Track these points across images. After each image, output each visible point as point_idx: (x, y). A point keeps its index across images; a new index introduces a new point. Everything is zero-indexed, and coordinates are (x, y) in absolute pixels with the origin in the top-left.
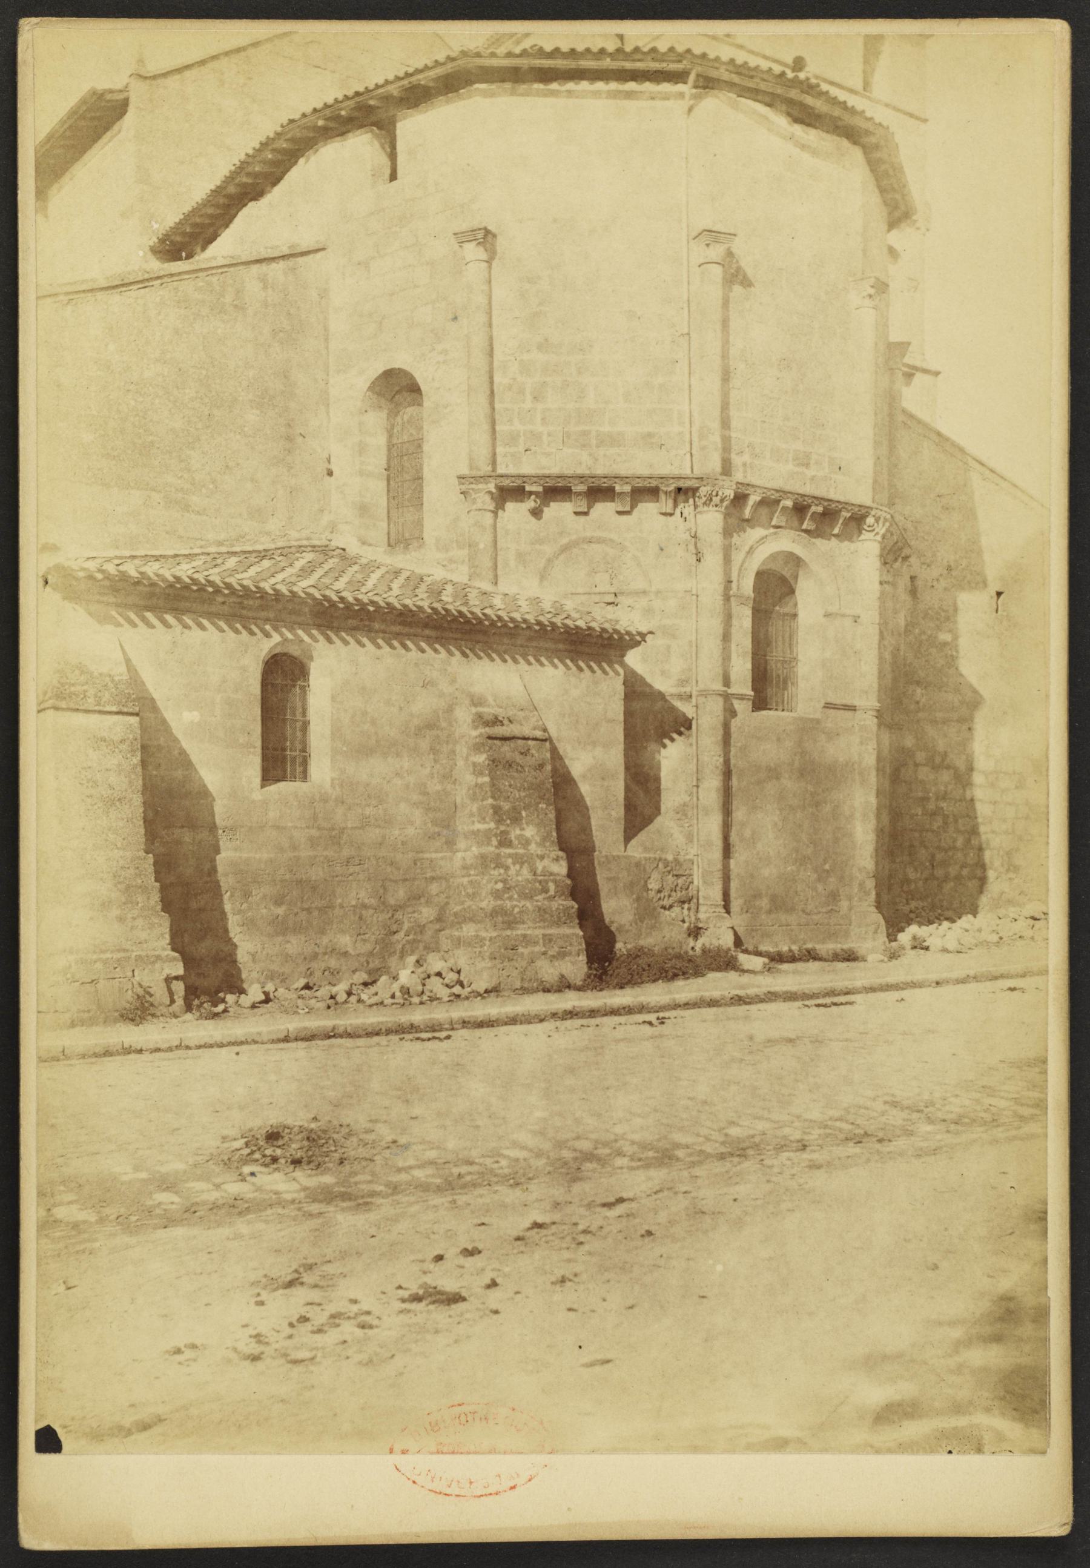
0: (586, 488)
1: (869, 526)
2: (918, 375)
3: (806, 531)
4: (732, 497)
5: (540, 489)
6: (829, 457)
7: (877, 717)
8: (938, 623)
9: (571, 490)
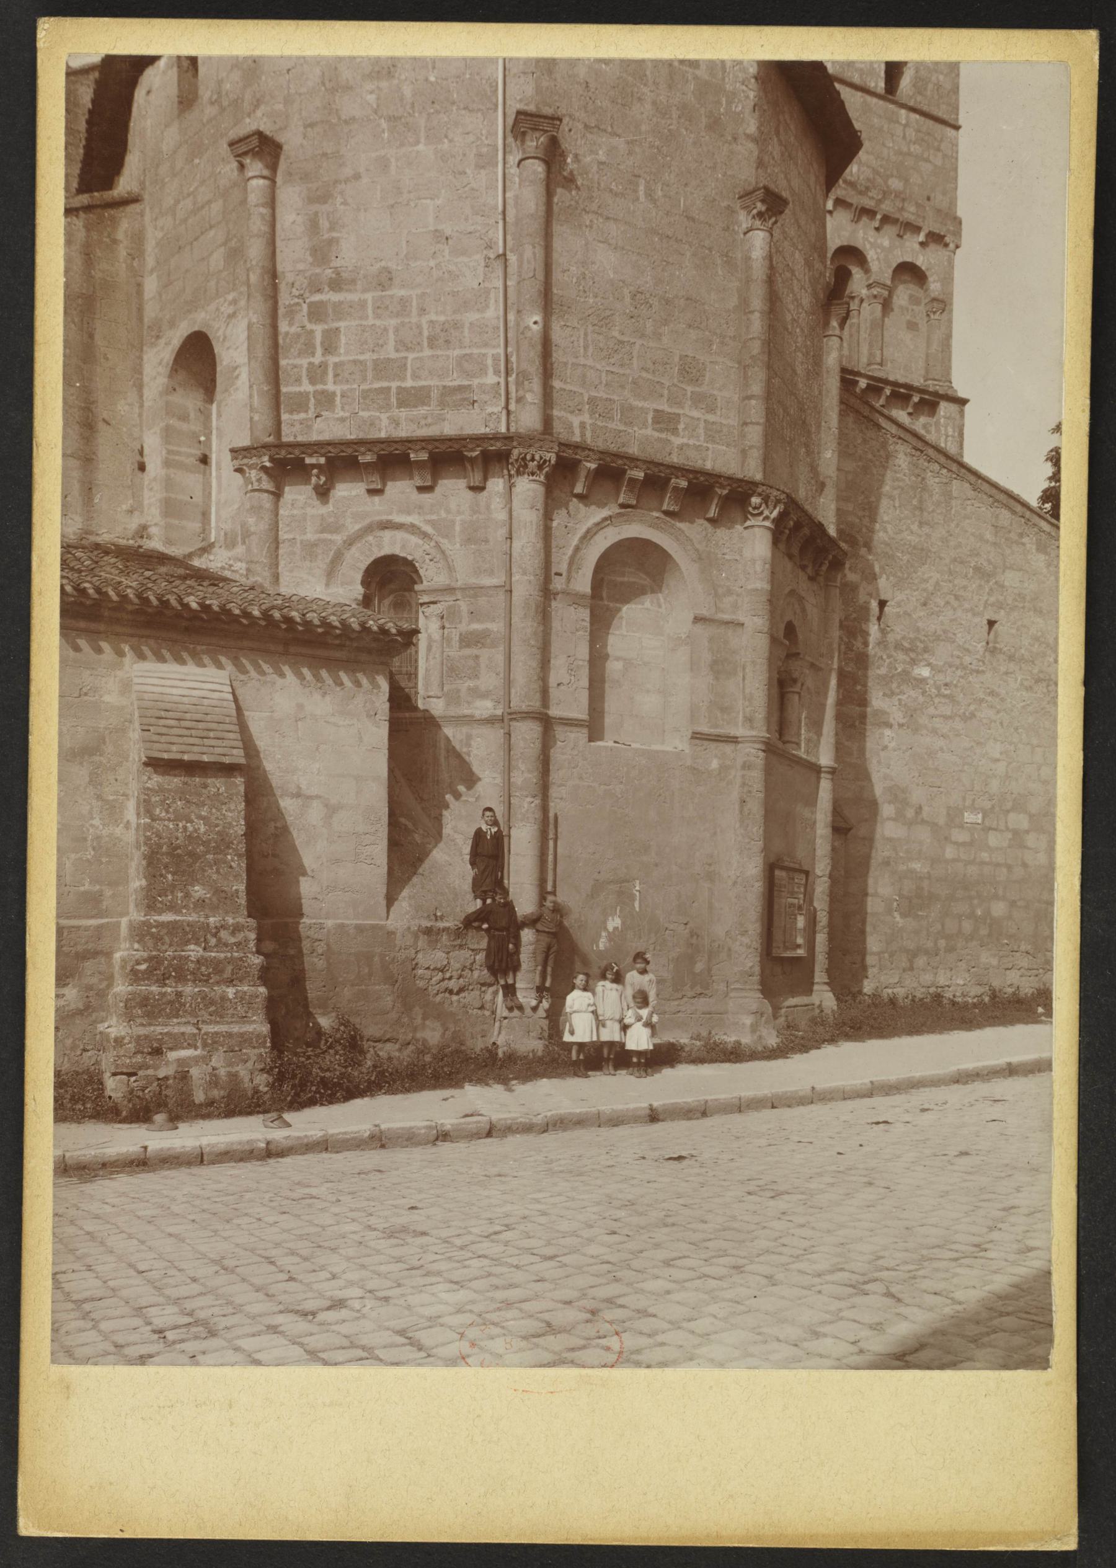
0: (375, 457)
1: (755, 508)
2: (943, 405)
3: (667, 513)
4: (553, 462)
5: (322, 460)
6: (705, 421)
7: (764, 751)
8: (913, 655)
9: (357, 462)
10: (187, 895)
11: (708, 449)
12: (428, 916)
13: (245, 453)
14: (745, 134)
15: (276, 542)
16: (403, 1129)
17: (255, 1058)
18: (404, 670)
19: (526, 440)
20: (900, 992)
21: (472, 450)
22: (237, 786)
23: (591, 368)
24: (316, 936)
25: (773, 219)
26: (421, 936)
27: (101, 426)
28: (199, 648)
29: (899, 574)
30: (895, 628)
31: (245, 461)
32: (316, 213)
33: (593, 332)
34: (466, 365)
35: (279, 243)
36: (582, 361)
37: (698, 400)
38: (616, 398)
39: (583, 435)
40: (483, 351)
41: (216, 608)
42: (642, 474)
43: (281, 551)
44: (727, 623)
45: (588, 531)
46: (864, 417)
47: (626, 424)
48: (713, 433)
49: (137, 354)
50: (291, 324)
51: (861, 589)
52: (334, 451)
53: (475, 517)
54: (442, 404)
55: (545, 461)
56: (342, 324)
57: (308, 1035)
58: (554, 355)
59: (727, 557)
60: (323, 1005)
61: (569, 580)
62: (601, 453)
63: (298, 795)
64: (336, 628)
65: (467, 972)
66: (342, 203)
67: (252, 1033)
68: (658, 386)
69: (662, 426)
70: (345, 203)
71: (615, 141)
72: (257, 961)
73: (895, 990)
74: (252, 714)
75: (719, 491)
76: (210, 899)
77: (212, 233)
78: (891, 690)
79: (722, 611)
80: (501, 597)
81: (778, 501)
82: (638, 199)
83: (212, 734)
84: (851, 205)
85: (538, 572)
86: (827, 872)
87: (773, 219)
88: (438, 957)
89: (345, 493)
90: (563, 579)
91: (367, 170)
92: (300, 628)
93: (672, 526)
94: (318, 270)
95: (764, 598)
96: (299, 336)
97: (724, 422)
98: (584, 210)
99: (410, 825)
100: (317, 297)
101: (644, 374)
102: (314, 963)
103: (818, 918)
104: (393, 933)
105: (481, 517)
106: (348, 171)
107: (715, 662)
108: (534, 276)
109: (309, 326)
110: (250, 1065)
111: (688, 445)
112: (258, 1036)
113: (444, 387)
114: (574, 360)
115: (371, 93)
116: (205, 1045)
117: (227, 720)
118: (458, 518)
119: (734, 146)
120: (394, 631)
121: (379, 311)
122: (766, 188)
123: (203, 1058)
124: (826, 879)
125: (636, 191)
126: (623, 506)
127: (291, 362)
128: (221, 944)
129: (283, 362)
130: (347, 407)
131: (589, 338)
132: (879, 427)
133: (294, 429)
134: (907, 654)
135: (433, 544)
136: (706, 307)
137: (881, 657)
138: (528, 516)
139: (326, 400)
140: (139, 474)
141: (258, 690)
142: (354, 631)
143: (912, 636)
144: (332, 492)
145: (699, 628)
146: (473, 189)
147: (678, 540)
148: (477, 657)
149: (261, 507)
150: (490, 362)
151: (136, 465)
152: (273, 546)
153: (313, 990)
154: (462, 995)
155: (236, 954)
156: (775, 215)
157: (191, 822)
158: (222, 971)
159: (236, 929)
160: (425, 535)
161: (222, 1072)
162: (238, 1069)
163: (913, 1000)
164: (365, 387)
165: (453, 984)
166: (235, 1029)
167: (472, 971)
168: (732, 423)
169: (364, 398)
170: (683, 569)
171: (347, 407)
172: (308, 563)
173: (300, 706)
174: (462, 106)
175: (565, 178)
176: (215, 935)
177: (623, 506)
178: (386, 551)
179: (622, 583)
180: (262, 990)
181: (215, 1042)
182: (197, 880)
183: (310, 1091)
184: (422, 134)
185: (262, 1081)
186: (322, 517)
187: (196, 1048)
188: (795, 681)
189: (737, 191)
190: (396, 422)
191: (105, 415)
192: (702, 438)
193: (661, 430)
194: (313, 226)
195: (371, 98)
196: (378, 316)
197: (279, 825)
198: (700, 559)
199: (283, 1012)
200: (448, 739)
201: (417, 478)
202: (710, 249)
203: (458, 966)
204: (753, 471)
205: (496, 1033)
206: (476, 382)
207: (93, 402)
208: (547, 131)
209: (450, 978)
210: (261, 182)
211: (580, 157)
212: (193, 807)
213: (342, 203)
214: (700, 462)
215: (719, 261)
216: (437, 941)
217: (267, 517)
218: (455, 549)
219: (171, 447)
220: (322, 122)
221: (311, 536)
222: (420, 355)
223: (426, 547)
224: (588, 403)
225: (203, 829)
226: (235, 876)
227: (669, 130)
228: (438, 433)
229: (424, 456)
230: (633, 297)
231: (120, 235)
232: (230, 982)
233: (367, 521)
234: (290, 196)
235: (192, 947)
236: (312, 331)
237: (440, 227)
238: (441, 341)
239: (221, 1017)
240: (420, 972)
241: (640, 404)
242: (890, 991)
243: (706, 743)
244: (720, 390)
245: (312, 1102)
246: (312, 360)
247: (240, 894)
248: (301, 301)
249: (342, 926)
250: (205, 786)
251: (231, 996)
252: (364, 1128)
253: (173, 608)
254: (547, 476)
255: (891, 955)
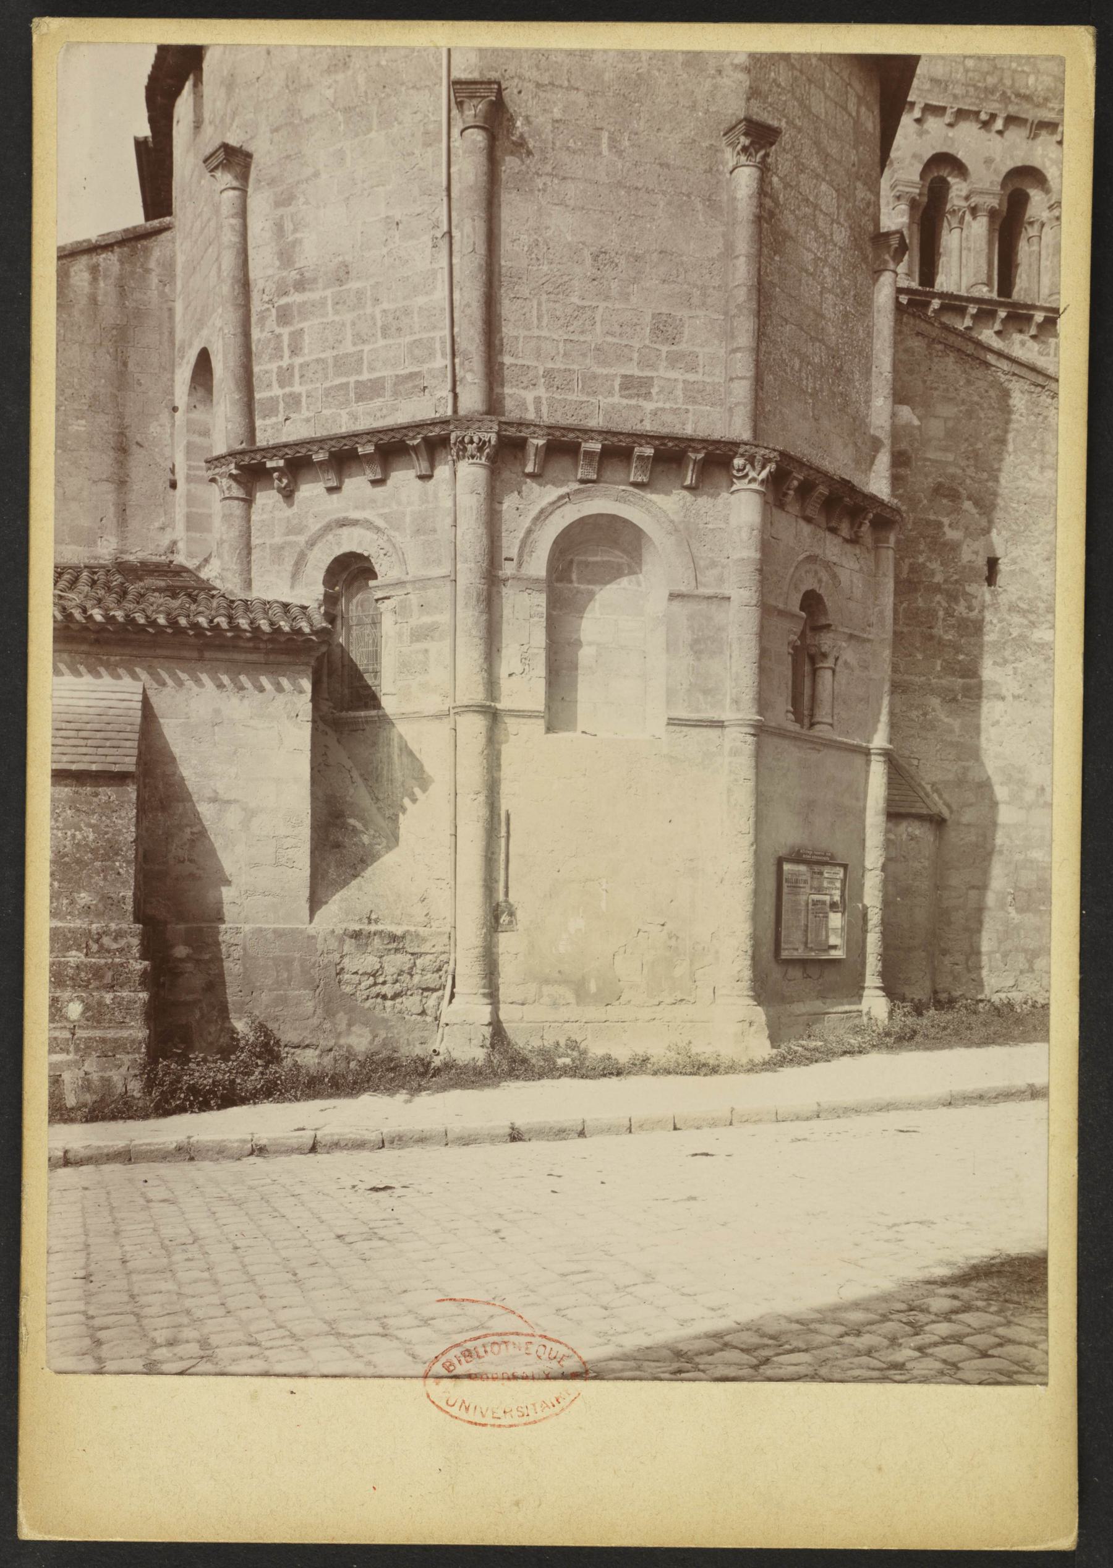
1: (739, 470)
4: (493, 442)
5: (281, 463)
8: (1033, 617)
10: (72, 902)
11: (687, 411)
12: (360, 919)
13: (216, 463)
14: (732, 64)
15: (248, 549)
16: (213, 1141)
17: (129, 1063)
18: (371, 667)
19: (465, 422)
20: (1016, 996)
21: (414, 438)
22: (129, 793)
23: (546, 338)
24: (232, 941)
25: (762, 153)
26: (348, 940)
27: (134, 448)
28: (112, 659)
29: (1014, 527)
30: (1009, 588)
31: (217, 470)
32: (282, 216)
33: (548, 300)
34: (416, 352)
35: (251, 253)
36: (536, 333)
37: (674, 360)
38: (575, 367)
39: (538, 410)
40: (432, 334)
41: (121, 619)
42: (600, 446)
43: (253, 557)
44: (709, 598)
45: (542, 511)
46: (968, 355)
47: (588, 394)
48: (694, 393)
49: (169, 376)
50: (262, 331)
51: (965, 547)
52: (290, 453)
53: (424, 507)
54: (396, 394)
55: (485, 442)
56: (305, 325)
57: (222, 1040)
58: (504, 329)
59: (710, 526)
60: (241, 1011)
61: (520, 565)
62: (549, 427)
63: (214, 800)
64: (245, 631)
65: (405, 977)
66: (304, 203)
67: (127, 1039)
68: (626, 350)
69: (630, 392)
70: (307, 203)
71: (574, 96)
72: (138, 967)
73: (1009, 995)
74: (167, 721)
75: (692, 455)
76: (96, 905)
77: (210, 250)
78: (1003, 658)
79: (705, 586)
80: (448, 588)
81: (769, 460)
82: (600, 153)
83: (108, 743)
84: (1026, 120)
85: (479, 558)
86: (880, 865)
87: (762, 153)
88: (370, 962)
89: (307, 494)
90: (514, 564)
91: (326, 166)
92: (209, 634)
93: (642, 498)
94: (285, 274)
95: (752, 568)
96: (269, 340)
97: (708, 380)
98: (538, 174)
99: (359, 825)
100: (284, 301)
101: (609, 339)
102: (232, 968)
103: (869, 917)
104: (313, 937)
105: (431, 506)
106: (309, 171)
107: (696, 641)
108: (474, 250)
109: (278, 330)
110: (123, 1070)
111: (663, 410)
112: (133, 1041)
113: (397, 376)
114: (527, 333)
115: (329, 87)
116: (77, 1050)
117: (129, 728)
118: (409, 509)
119: (719, 79)
120: (307, 630)
121: (338, 307)
122: (748, 120)
123: (76, 1062)
124: (878, 872)
125: (598, 145)
126: (583, 481)
127: (262, 368)
128: (102, 949)
129: (256, 369)
130: (311, 407)
131: (544, 308)
132: (987, 365)
133: (267, 434)
134: (1024, 616)
135: (385, 538)
136: (684, 258)
137: (991, 622)
138: (471, 503)
139: (294, 401)
140: (171, 491)
141: (173, 697)
142: (264, 633)
143: (1031, 595)
144: (297, 494)
145: (676, 605)
146: (421, 169)
147: (649, 512)
148: (426, 651)
149: (231, 514)
150: (438, 346)
151: (168, 483)
152: (244, 552)
153: (233, 994)
154: (399, 1000)
155: (117, 960)
156: (762, 147)
157: (80, 830)
158: (102, 977)
159: (118, 935)
160: (378, 530)
161: (95, 1077)
162: (111, 1074)
163: (1033, 1006)
164: (328, 384)
165: (387, 990)
166: (111, 1034)
167: (412, 976)
168: (717, 380)
169: (327, 396)
170: (657, 542)
171: (311, 407)
172: (276, 566)
173: (217, 711)
174: (411, 85)
175: (514, 143)
176: (97, 941)
177: (583, 481)
178: (345, 548)
179: (597, 563)
180: (144, 996)
181: (87, 1047)
182: (83, 887)
183: (179, 1099)
184: (375, 121)
185: (135, 1087)
186: (288, 520)
187: (68, 1053)
188: (825, 656)
189: (721, 127)
190: (354, 417)
191: (138, 438)
192: (680, 401)
193: (630, 397)
194: (279, 228)
195: (329, 93)
196: (337, 312)
197: (195, 830)
198: (676, 530)
199: (198, 1016)
200: (401, 736)
201: (368, 471)
202: (689, 195)
203: (393, 970)
204: (739, 429)
205: (439, 1040)
206: (426, 367)
207: (126, 428)
208: (484, 97)
209: (384, 983)
210: (231, 193)
211: (531, 119)
212: (83, 816)
213: (304, 203)
214: (678, 426)
215: (699, 206)
216: (367, 945)
217: (238, 523)
218: (404, 540)
219: (193, 464)
220: (286, 124)
221: (278, 540)
222: (376, 346)
223: (381, 542)
224: (544, 376)
225: (91, 837)
226: (123, 883)
227: (638, 75)
228: (392, 423)
229: (596, 447)
230: (595, 258)
231: (152, 264)
232: (111, 987)
233: (324, 522)
234: (259, 202)
235: (74, 953)
236: (279, 336)
237: (390, 214)
238: (393, 329)
239: (99, 1022)
240: (346, 977)
241: (605, 371)
242: (1003, 995)
243: (685, 729)
244: (702, 346)
245: (181, 1110)
246: (280, 363)
247: (127, 900)
248: (270, 306)
249: (261, 930)
250: (96, 795)
251: (108, 1002)
252: (120, 1144)
253: (77, 622)
254: (488, 457)
255: (1005, 955)
